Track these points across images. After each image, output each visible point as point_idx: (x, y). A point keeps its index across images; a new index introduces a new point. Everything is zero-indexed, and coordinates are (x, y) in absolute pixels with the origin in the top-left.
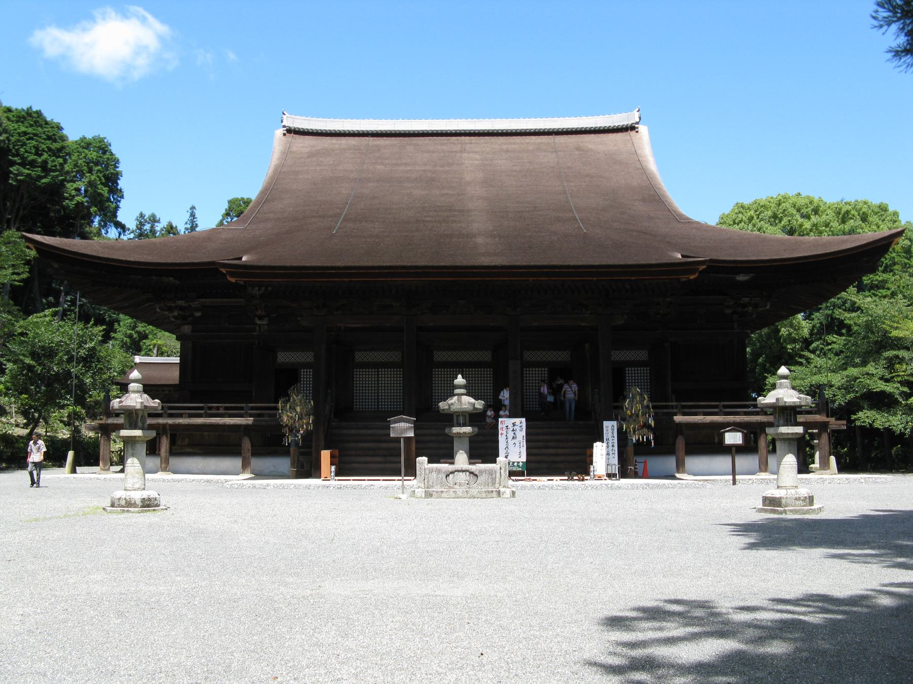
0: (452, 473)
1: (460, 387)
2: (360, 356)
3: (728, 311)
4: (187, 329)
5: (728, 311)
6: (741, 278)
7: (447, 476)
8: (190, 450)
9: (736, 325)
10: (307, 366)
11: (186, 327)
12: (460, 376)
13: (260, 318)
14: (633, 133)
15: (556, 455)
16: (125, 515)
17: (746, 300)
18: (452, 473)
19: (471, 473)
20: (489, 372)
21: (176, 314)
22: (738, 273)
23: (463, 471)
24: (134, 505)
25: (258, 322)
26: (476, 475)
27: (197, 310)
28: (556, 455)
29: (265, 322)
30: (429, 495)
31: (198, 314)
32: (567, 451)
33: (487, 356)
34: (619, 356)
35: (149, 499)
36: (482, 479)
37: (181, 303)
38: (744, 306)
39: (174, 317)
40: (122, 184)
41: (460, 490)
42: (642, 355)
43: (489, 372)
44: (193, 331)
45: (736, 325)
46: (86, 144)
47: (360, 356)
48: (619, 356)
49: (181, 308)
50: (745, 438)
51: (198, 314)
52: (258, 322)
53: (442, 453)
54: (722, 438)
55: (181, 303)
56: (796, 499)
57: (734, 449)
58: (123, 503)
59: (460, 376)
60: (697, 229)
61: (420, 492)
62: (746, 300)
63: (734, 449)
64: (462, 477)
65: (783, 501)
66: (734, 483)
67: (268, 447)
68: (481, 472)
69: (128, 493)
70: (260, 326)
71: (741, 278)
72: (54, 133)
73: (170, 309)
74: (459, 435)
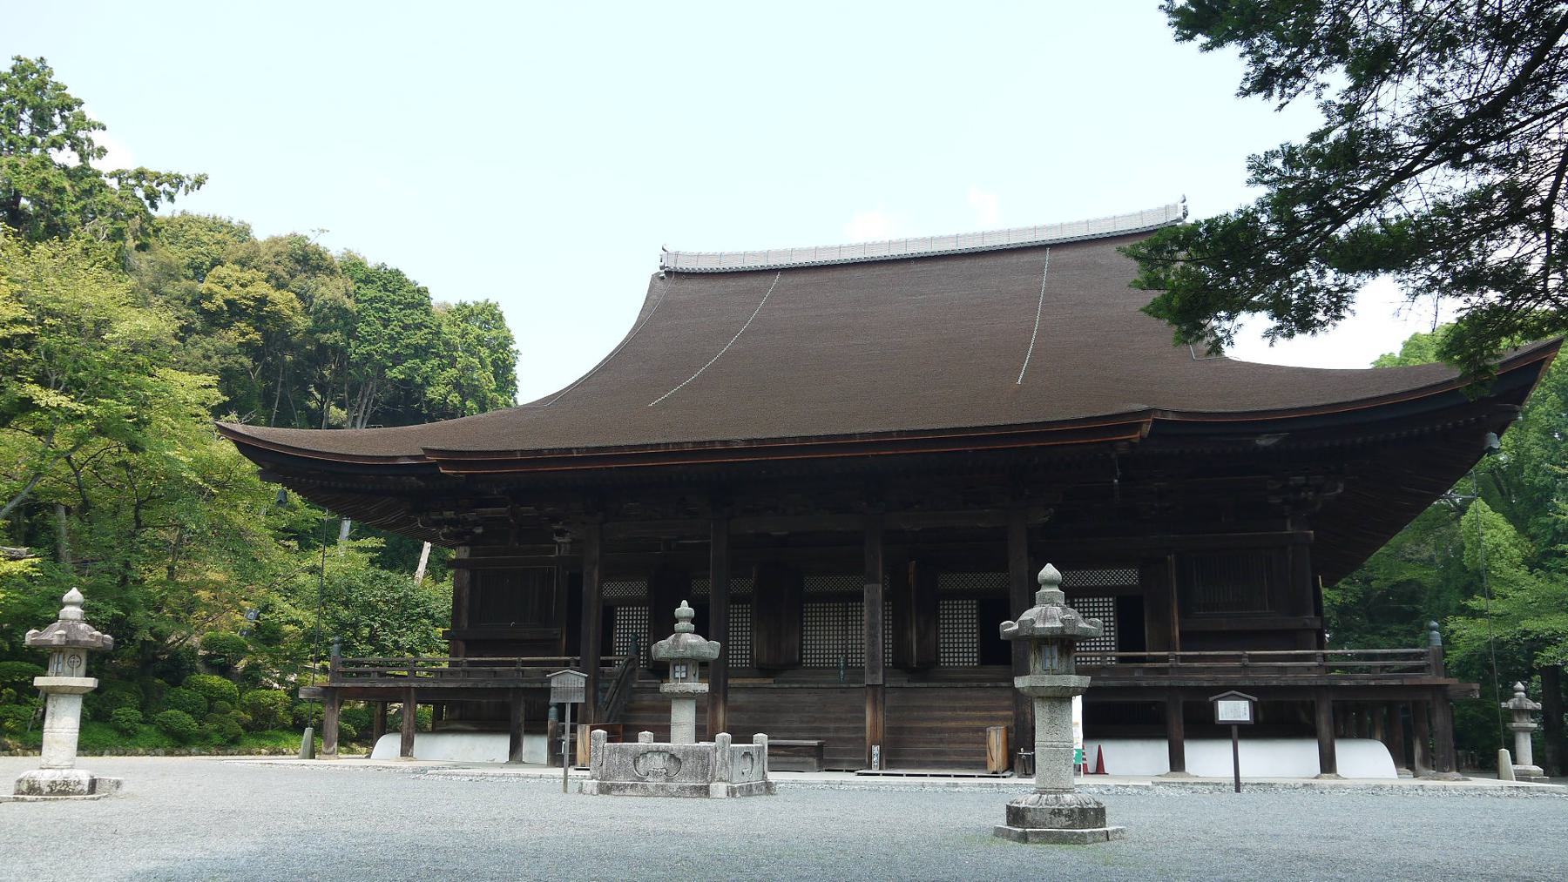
2: (813, 584)
3: (1275, 500)
5: (1275, 500)
12: (684, 602)
13: (560, 533)
14: (672, 265)
17: (1300, 479)
19: (672, 756)
22: (1258, 434)
25: (557, 539)
28: (943, 719)
29: (566, 540)
30: (605, 790)
31: (479, 530)
34: (613, 590)
35: (67, 783)
37: (449, 514)
41: (652, 782)
42: (639, 588)
46: (466, 314)
47: (813, 584)
48: (613, 590)
49: (450, 522)
51: (479, 530)
52: (557, 539)
54: (1213, 710)
55: (449, 514)
56: (1053, 812)
57: (1235, 730)
58: (24, 787)
59: (684, 602)
61: (591, 785)
62: (1300, 479)
63: (1235, 730)
65: (1029, 816)
66: (1238, 790)
71: (1263, 442)
72: (418, 300)
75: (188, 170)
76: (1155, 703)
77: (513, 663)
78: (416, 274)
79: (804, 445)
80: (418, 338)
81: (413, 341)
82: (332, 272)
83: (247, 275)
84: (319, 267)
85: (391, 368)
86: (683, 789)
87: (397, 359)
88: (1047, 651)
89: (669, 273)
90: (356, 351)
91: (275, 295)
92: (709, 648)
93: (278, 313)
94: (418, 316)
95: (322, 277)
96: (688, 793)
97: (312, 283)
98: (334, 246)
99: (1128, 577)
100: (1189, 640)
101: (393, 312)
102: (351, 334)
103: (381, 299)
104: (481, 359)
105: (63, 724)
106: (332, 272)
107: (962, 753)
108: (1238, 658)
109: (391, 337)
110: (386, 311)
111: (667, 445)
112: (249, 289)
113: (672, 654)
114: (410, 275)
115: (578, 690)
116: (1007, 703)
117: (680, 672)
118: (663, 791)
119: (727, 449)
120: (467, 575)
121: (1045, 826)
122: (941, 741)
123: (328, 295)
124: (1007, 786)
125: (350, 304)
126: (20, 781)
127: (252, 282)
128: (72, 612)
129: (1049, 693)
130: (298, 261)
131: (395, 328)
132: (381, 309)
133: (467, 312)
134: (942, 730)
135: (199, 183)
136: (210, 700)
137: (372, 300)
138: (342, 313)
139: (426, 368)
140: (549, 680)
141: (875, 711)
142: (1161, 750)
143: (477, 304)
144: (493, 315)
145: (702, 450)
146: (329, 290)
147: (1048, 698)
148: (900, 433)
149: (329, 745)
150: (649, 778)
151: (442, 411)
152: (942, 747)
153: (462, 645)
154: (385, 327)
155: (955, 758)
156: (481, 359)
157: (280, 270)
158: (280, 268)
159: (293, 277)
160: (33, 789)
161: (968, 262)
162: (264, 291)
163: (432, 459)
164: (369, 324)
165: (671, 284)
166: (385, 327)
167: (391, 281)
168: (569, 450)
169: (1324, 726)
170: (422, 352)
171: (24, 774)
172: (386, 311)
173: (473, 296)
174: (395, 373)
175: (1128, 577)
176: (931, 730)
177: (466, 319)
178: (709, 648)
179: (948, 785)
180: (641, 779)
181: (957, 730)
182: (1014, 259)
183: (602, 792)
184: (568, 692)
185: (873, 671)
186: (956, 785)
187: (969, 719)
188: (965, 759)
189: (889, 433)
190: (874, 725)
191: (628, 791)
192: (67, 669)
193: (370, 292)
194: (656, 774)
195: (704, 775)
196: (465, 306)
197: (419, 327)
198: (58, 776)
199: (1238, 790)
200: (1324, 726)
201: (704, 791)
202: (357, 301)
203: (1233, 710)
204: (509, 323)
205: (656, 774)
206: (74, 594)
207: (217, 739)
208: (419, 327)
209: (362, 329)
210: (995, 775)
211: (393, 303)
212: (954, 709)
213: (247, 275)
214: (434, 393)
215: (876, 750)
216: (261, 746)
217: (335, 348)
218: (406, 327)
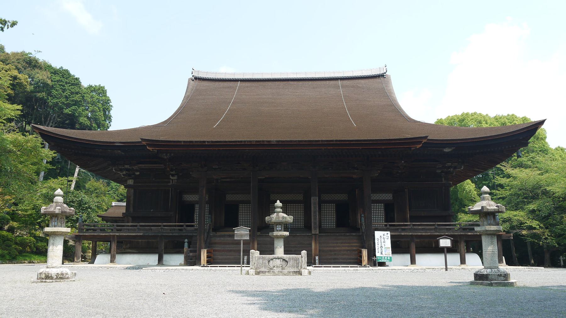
0: (272, 259)
1: (278, 207)
3: (439, 171)
4: (131, 182)
6: (447, 150)
7: (269, 261)
8: (134, 251)
9: (443, 179)
10: (197, 202)
11: (131, 180)
12: (278, 201)
13: (173, 175)
14: (196, 75)
15: (334, 247)
16: (43, 284)
17: (449, 164)
18: (272, 259)
19: (284, 260)
20: (302, 206)
21: (124, 173)
22: (445, 148)
23: (278, 258)
24: (51, 278)
25: (171, 178)
26: (287, 261)
27: (137, 171)
28: (334, 247)
29: (175, 178)
30: (258, 273)
31: (138, 173)
32: (347, 248)
33: (300, 197)
35: (62, 274)
36: (291, 263)
37: (126, 166)
38: (449, 167)
39: (123, 175)
40: (112, 113)
43: (302, 206)
44: (134, 183)
45: (443, 179)
46: (91, 89)
49: (127, 170)
50: (452, 242)
51: (138, 173)
52: (171, 178)
53: (267, 249)
54: (438, 243)
55: (126, 166)
58: (43, 276)
59: (278, 201)
60: (419, 125)
61: (252, 272)
62: (449, 164)
63: (445, 249)
64: (278, 262)
65: (490, 277)
67: (159, 246)
68: (289, 259)
69: (48, 270)
70: (172, 180)
71: (447, 150)
72: (76, 82)
73: (121, 170)
74: (278, 237)
75: (9, 18)
76: (398, 241)
77: (160, 226)
78: (74, 72)
79: (310, 143)
80: (77, 98)
81: (75, 99)
82: (41, 68)
83: (7, 67)
84: (35, 66)
85: (66, 109)
86: (290, 272)
87: (68, 106)
88: (488, 217)
89: (196, 78)
90: (51, 101)
91: (20, 76)
92: (289, 219)
93: (21, 83)
94: (77, 89)
95: (37, 70)
96: (291, 273)
97: (33, 72)
98: (41, 57)
99: (388, 197)
100: (413, 219)
101: (67, 86)
102: (49, 94)
103: (61, 81)
104: (99, 108)
105: (56, 250)
106: (41, 68)
107: (344, 259)
108: (433, 225)
109: (66, 97)
110: (64, 86)
111: (245, 141)
112: (9, 72)
113: (277, 221)
114: (72, 73)
115: (246, 234)
116: (355, 241)
117: (279, 228)
118: (281, 273)
119: (269, 144)
120: (132, 191)
121: (496, 280)
122: (335, 254)
123: (41, 78)
124: (376, 270)
125: (49, 82)
126: (41, 274)
127: (10, 70)
128: (60, 199)
129: (489, 233)
130: (27, 63)
131: (67, 93)
132: (62, 85)
133: (92, 89)
134: (334, 251)
135: (14, 24)
136: (4, 241)
137: (58, 81)
138: (45, 85)
139: (80, 109)
140: (234, 231)
141: (316, 243)
142: (408, 257)
143: (96, 86)
144: (103, 91)
145: (259, 144)
146: (41, 76)
147: (490, 234)
148: (336, 141)
149: (78, 259)
150: (275, 268)
151: (83, 127)
152: (335, 257)
153: (130, 219)
154: (63, 92)
155: (341, 261)
156: (99, 108)
157: (19, 66)
158: (20, 65)
159: (25, 69)
160: (48, 277)
161: (310, 82)
162: (16, 74)
163: (144, 143)
164: (57, 90)
165: (197, 82)
166: (63, 92)
167: (64, 74)
168: (204, 142)
169: (413, 249)
170: (76, 103)
171: (41, 271)
172: (64, 86)
173: (95, 83)
174: (67, 111)
175: (388, 197)
176: (331, 251)
177: (92, 91)
178: (289, 219)
179: (354, 270)
180: (272, 269)
181: (340, 251)
182: (328, 82)
183: (256, 274)
184: (242, 235)
185: (315, 229)
186: (357, 270)
187: (343, 246)
188: (345, 261)
189: (319, 141)
190: (316, 249)
191: (267, 274)
192: (59, 224)
193: (58, 78)
194: (277, 267)
195: (297, 267)
196: (91, 86)
197: (77, 93)
198: (59, 271)
199: (446, 269)
200: (413, 249)
201: (300, 273)
202: (52, 81)
203: (445, 243)
204: (108, 94)
205: (277, 267)
206: (59, 191)
207: (8, 257)
208: (77, 93)
209: (54, 92)
210: (365, 266)
211: (66, 83)
212: (337, 243)
213: (7, 67)
214: (82, 120)
215: (317, 258)
216: (25, 260)
217: (42, 99)
218: (72, 93)
